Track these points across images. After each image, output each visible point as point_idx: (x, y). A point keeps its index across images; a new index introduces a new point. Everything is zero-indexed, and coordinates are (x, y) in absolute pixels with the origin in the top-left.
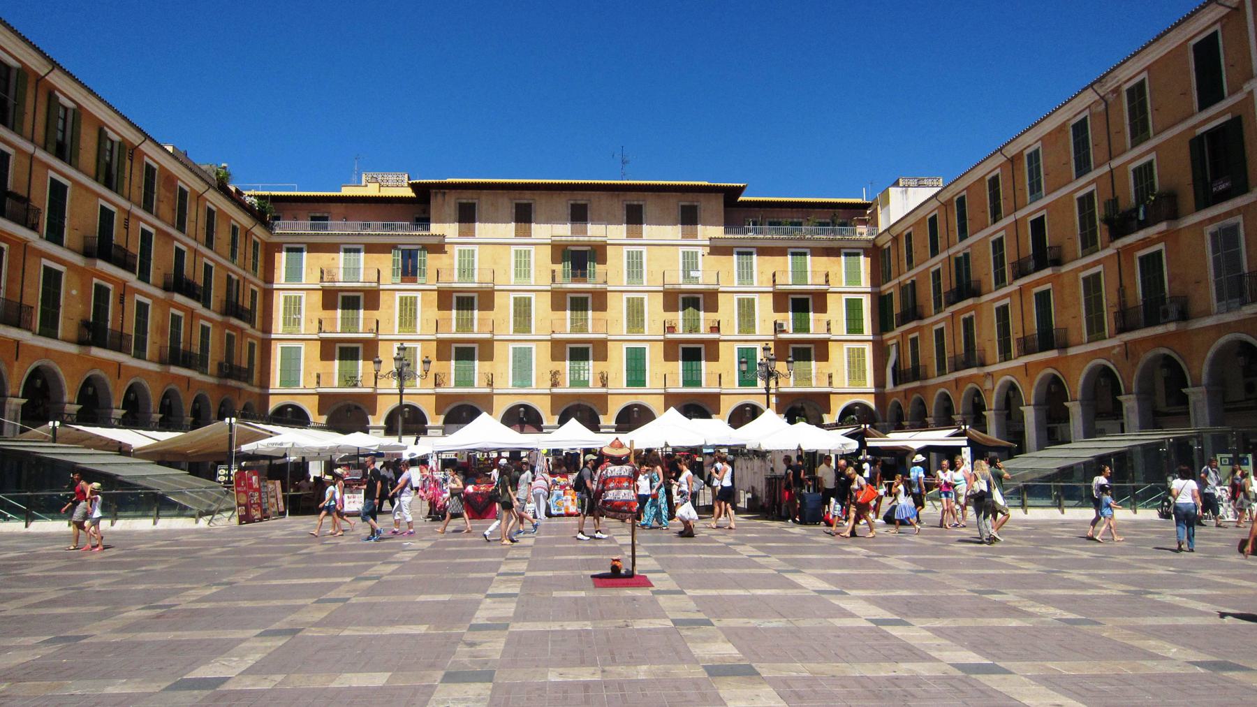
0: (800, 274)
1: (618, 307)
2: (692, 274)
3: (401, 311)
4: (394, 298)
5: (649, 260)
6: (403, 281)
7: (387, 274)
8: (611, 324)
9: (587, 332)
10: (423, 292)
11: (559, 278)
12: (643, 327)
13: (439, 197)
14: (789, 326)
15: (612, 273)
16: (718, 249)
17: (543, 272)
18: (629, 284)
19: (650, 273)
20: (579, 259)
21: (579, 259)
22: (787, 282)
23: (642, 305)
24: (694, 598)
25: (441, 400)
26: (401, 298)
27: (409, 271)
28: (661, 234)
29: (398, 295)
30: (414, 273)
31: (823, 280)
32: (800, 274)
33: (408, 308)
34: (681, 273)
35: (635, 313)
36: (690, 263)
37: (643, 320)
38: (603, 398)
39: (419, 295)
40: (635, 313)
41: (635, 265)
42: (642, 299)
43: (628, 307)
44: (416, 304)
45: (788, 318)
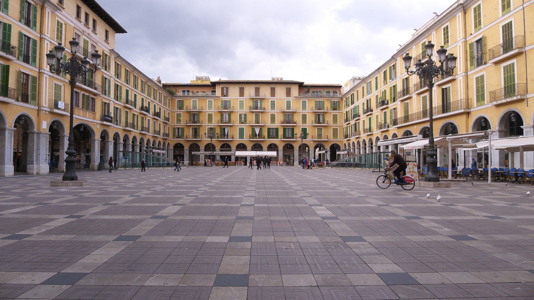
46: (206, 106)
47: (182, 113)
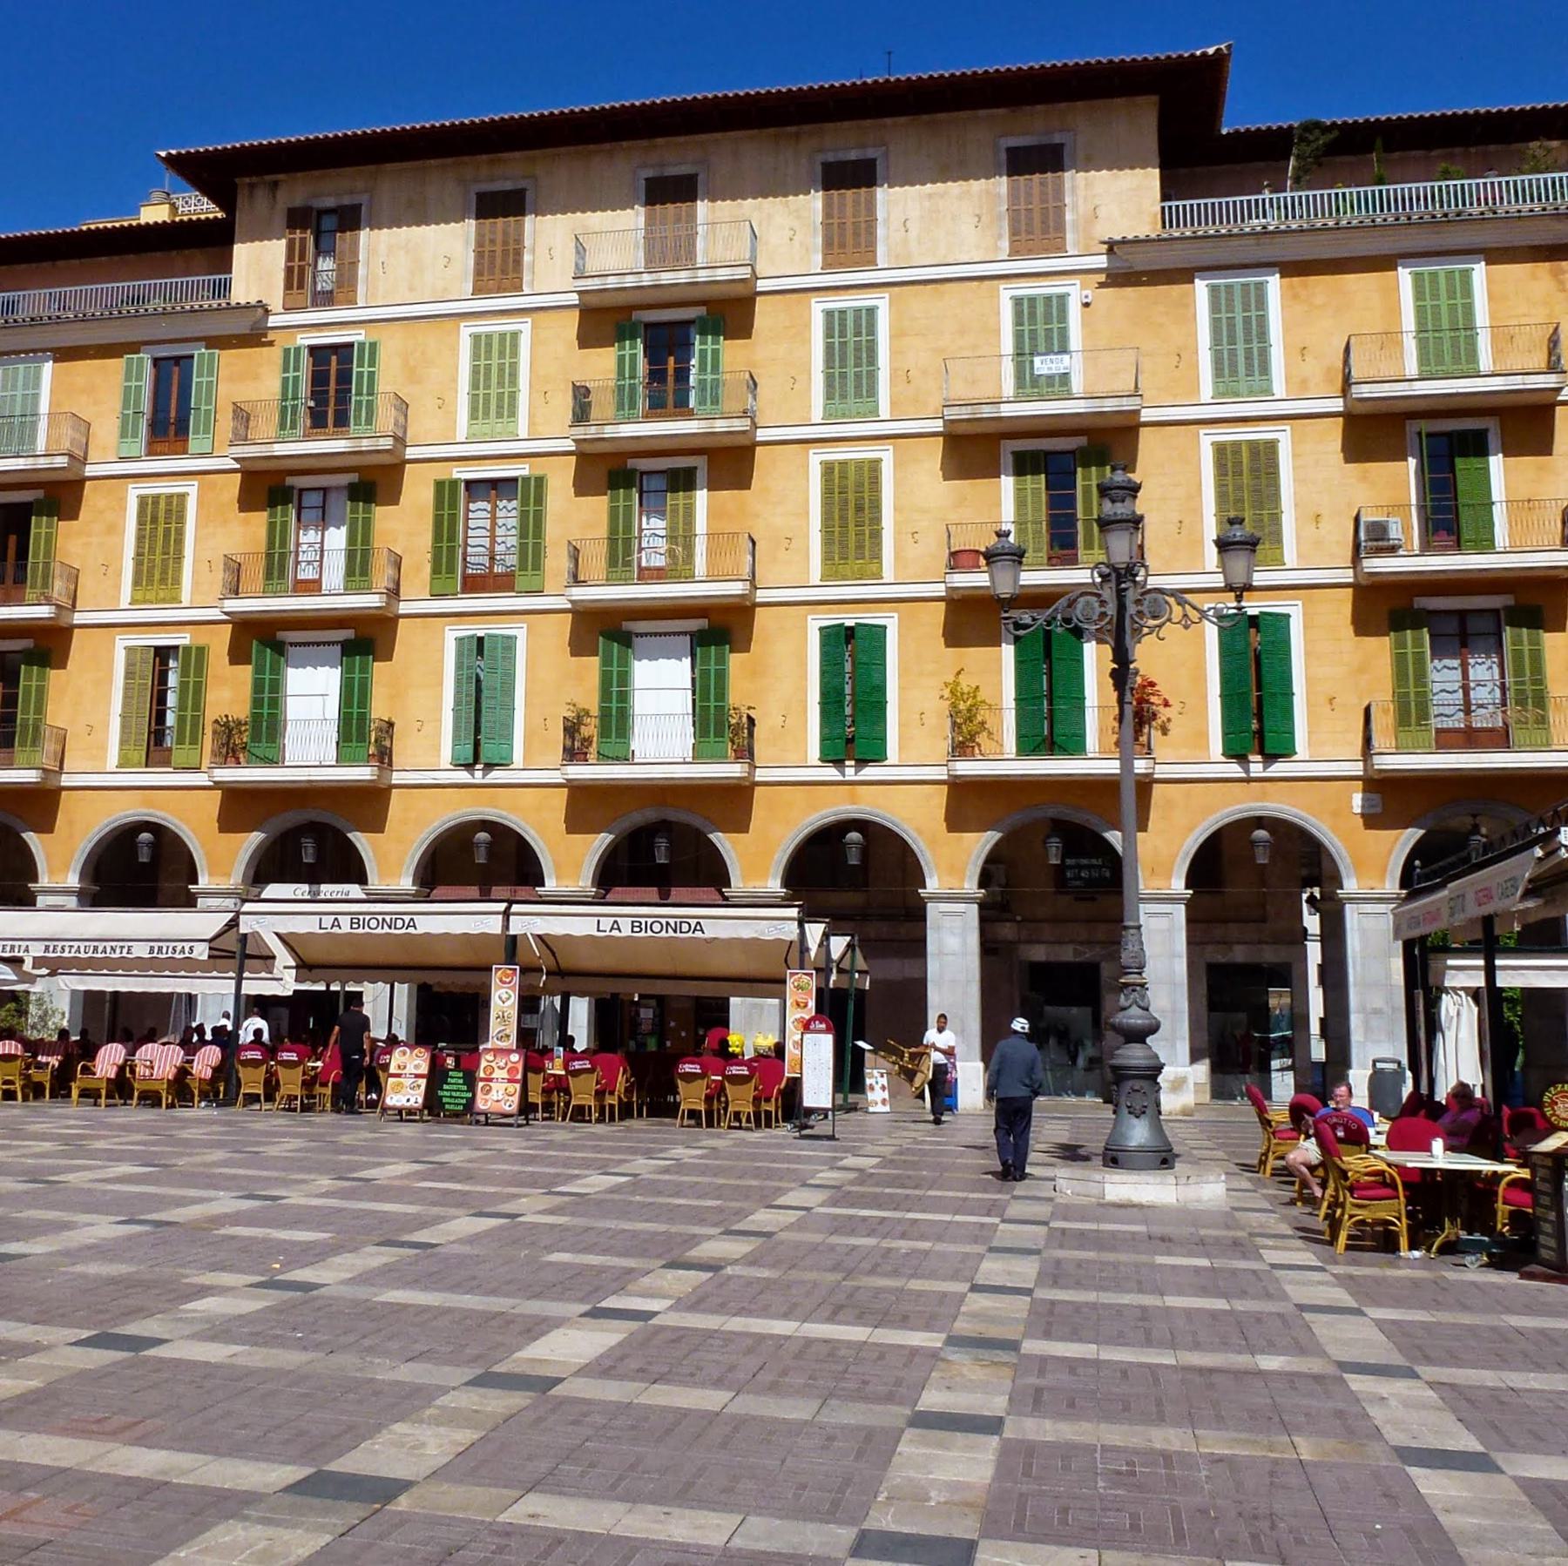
0: (1447, 336)
1: (789, 498)
2: (1043, 365)
3: (140, 538)
4: (123, 500)
5: (896, 335)
6: (152, 452)
7: (106, 431)
8: (768, 531)
9: (689, 578)
10: (201, 477)
11: (602, 406)
12: (877, 556)
13: (261, 195)
14: (1407, 526)
15: (776, 379)
16: (1130, 268)
17: (555, 393)
18: (830, 416)
19: (903, 376)
20: (666, 333)
21: (666, 333)
22: (1402, 373)
23: (875, 481)
24: (1379, 1323)
25: (240, 806)
26: (143, 501)
27: (168, 425)
28: (940, 220)
29: (134, 492)
30: (182, 429)
31: (1539, 359)
32: (1447, 336)
33: (161, 521)
34: (1008, 368)
35: (852, 510)
36: (1040, 326)
37: (876, 535)
38: (733, 803)
39: (191, 489)
40: (852, 510)
41: (851, 357)
42: (875, 465)
43: (828, 492)
44: (181, 519)
45: (1399, 482)
46: (1184, 356)
47: (886, 455)
